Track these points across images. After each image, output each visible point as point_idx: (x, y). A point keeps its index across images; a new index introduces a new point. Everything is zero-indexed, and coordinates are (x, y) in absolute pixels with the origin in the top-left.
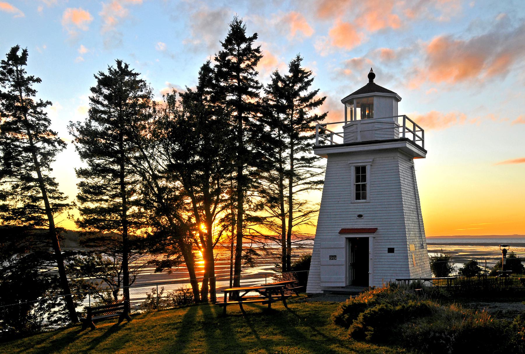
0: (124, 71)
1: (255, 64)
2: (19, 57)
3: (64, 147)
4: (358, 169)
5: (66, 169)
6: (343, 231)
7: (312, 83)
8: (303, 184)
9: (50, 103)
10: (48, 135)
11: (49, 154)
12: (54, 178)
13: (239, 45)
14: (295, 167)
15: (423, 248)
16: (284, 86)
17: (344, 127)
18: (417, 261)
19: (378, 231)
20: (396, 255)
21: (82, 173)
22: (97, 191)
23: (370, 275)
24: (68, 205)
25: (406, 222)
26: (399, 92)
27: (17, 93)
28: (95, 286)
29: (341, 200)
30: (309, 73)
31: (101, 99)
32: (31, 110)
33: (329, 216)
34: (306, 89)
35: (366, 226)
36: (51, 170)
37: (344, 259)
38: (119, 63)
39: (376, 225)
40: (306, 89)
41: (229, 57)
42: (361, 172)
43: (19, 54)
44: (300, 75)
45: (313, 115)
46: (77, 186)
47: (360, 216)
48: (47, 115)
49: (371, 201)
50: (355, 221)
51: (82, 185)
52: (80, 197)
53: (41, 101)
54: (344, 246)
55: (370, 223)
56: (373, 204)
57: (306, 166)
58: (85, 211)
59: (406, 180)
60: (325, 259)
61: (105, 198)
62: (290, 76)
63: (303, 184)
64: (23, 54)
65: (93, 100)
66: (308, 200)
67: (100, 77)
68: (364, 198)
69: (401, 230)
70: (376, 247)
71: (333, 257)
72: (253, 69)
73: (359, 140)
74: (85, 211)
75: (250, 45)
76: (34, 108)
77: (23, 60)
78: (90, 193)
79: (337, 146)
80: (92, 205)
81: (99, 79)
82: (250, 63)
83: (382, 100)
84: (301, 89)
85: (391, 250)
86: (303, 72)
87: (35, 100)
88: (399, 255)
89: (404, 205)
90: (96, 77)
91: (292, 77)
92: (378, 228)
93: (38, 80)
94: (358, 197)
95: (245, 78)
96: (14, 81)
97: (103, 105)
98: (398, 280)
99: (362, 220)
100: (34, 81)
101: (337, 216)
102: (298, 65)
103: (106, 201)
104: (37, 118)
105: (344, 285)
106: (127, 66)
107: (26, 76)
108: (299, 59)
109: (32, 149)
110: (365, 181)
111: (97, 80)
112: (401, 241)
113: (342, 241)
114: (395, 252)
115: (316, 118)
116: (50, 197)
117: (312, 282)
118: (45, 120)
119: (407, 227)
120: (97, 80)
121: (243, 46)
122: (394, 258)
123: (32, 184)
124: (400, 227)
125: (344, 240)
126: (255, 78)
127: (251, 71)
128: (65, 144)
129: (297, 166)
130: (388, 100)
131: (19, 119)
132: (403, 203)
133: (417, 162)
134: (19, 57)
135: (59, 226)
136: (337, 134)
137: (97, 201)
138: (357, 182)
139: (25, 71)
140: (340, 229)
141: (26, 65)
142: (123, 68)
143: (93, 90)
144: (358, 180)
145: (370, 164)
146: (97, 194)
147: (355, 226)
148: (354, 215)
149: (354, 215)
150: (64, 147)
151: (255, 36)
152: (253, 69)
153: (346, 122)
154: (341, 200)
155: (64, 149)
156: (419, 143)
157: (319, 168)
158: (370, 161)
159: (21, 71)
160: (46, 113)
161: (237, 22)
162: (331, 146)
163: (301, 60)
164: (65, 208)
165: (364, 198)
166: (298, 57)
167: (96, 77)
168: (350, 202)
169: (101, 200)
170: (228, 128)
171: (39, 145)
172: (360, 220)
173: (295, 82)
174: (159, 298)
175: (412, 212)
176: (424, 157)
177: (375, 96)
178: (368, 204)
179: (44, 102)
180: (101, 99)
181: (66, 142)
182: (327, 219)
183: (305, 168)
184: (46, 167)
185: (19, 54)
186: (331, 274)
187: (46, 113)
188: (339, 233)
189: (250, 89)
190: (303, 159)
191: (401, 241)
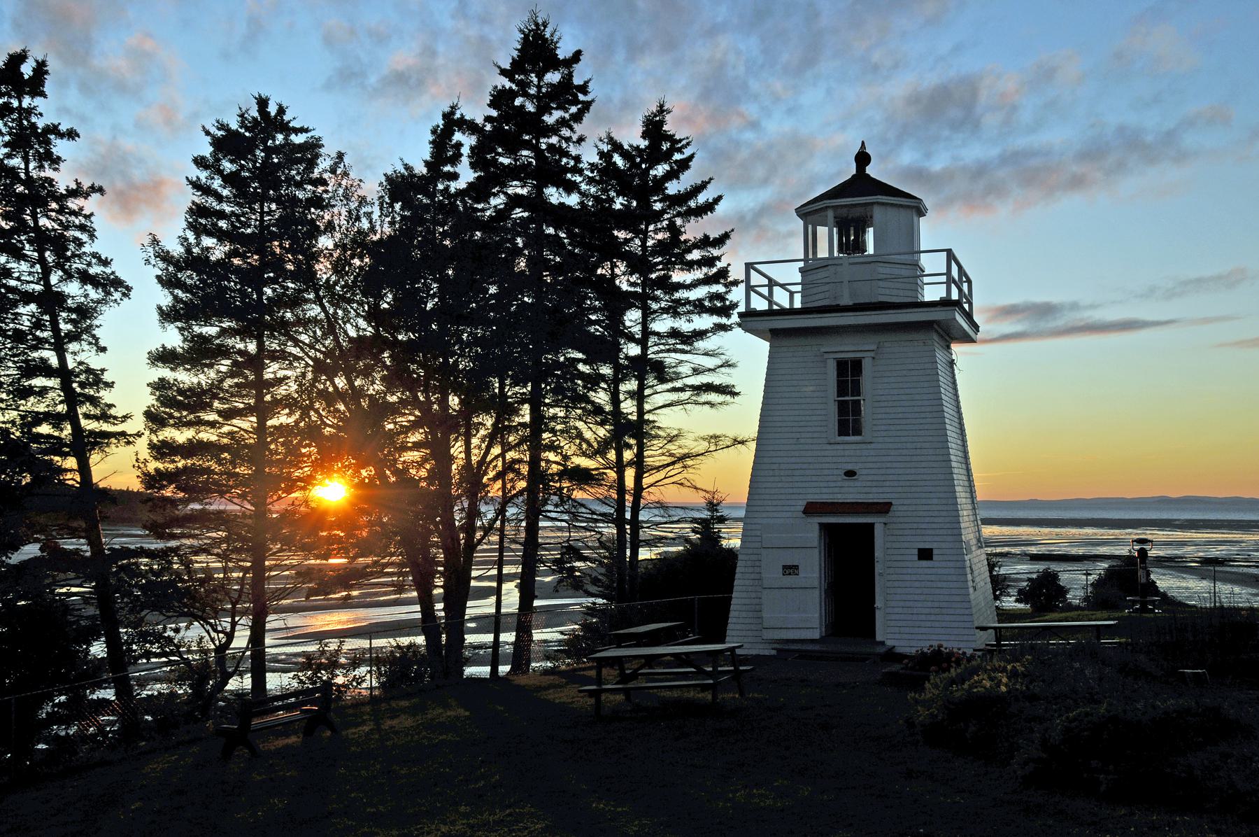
0: (268, 122)
1: (578, 117)
2: (26, 77)
3: (124, 295)
4: (842, 366)
5: (130, 346)
6: (812, 509)
8: (668, 391)
9: (101, 190)
10: (89, 264)
11: (84, 312)
12: (103, 370)
13: (540, 77)
16: (629, 169)
17: (801, 270)
20: (937, 564)
21: (165, 357)
22: (196, 400)
23: (877, 612)
24: (123, 434)
27: (16, 162)
28: (172, 634)
29: (804, 435)
30: (684, 142)
31: (217, 183)
32: (54, 205)
33: (777, 473)
34: (678, 178)
35: (862, 496)
36: (104, 349)
37: (816, 575)
38: (262, 103)
39: (888, 496)
40: (678, 178)
41: (518, 102)
42: (849, 372)
43: (27, 70)
44: (665, 146)
45: (700, 236)
46: (149, 390)
47: (850, 474)
48: (93, 219)
50: (839, 484)
51: (160, 386)
52: (149, 415)
53: (78, 184)
54: (816, 543)
55: (874, 490)
56: (880, 446)
57: (676, 351)
58: (162, 450)
60: (773, 574)
61: (212, 417)
62: (642, 147)
63: (668, 391)
64: (34, 70)
65: (196, 185)
66: (685, 428)
67: (220, 133)
68: (857, 432)
69: (946, 508)
70: (888, 545)
71: (790, 570)
72: (572, 129)
73: (846, 301)
74: (162, 450)
75: (570, 75)
76: (60, 199)
77: (36, 86)
78: (180, 406)
79: (783, 312)
80: (182, 436)
81: (213, 136)
82: (567, 116)
83: (891, 212)
84: (672, 175)
85: (925, 554)
86: (670, 138)
87: (63, 180)
88: (944, 564)
90: (208, 133)
91: (647, 147)
93: (72, 134)
94: (843, 430)
95: (551, 147)
96: (10, 134)
97: (220, 198)
100: (61, 135)
101: (797, 473)
102: (662, 123)
103: (212, 424)
104: (61, 224)
106: (281, 111)
107: (41, 123)
108: (662, 110)
109: (51, 301)
111: (209, 139)
112: (949, 532)
113: (811, 531)
114: (935, 557)
115: (705, 242)
116: (87, 416)
117: (738, 627)
118: (82, 228)
120: (209, 139)
121: (553, 77)
122: (934, 571)
123: (39, 382)
124: (944, 502)
125: (817, 527)
126: (573, 150)
127: (565, 132)
128: (129, 289)
129: (656, 348)
130: (903, 214)
131: (22, 227)
133: (957, 349)
134: (26, 77)
135: (101, 485)
136: (783, 286)
137: (189, 424)
139: (39, 110)
140: (805, 503)
141: (45, 96)
142: (273, 114)
143: (200, 162)
144: (842, 390)
145: (872, 354)
146: (192, 409)
147: (839, 496)
148: (836, 472)
149: (836, 472)
150: (124, 295)
152: (572, 129)
153: (806, 260)
154: (804, 435)
155: (126, 300)
157: (706, 354)
158: (873, 347)
159: (30, 111)
160: (92, 214)
162: (770, 313)
163: (669, 112)
164: (113, 440)
165: (857, 432)
166: (661, 106)
167: (208, 133)
168: (825, 441)
169: (199, 423)
170: (520, 262)
171: (73, 289)
172: (851, 484)
173: (653, 163)
174: (222, 649)
177: (878, 203)
178: (869, 446)
179: (86, 185)
180: (217, 183)
181: (129, 283)
182: (771, 479)
183: (673, 355)
184: (90, 343)
185: (27, 70)
186: (779, 609)
187: (92, 214)
188: (805, 512)
190: (674, 333)
191: (949, 532)
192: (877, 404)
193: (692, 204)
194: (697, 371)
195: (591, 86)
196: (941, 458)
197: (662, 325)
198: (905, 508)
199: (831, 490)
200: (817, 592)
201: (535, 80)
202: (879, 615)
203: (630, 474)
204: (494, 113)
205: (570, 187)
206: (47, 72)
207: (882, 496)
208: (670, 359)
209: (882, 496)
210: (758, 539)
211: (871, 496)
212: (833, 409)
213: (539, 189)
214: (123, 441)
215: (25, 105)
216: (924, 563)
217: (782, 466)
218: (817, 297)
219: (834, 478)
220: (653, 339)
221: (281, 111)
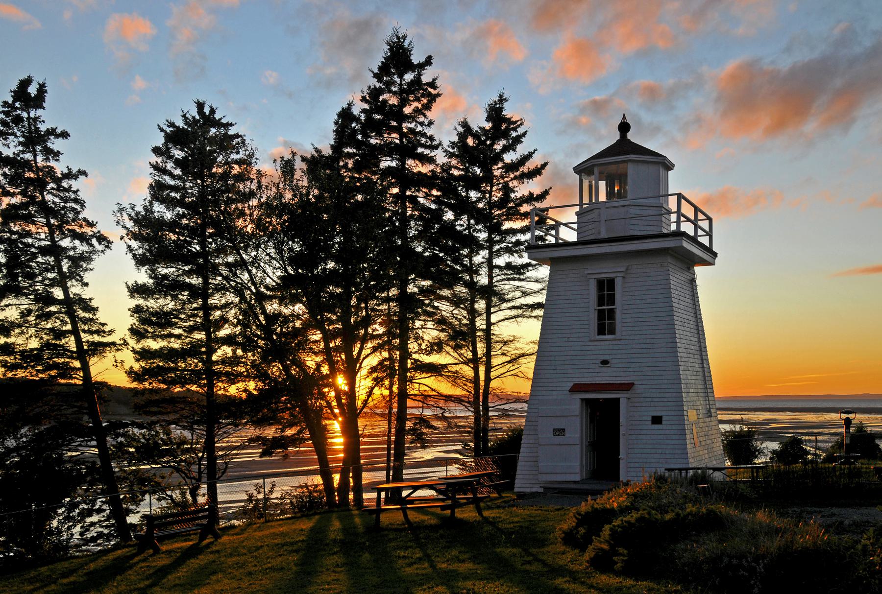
1: (428, 107)
2: (33, 95)
3: (107, 247)
4: (601, 284)
5: (112, 285)
6: (577, 388)
7: (523, 139)
8: (509, 308)
9: (84, 173)
12: (90, 299)
13: (401, 76)
14: (495, 279)
15: (711, 416)
16: (478, 145)
17: (577, 214)
18: (701, 439)
19: (634, 387)
21: (137, 290)
25: (681, 372)
26: (670, 155)
27: (28, 156)
28: (160, 480)
31: (170, 166)
32: (52, 185)
34: (514, 150)
35: (614, 379)
36: (86, 284)
37: (578, 435)
38: (200, 106)
40: (514, 150)
42: (606, 288)
43: (33, 90)
45: (526, 193)
46: (130, 313)
47: (605, 362)
48: (79, 193)
49: (624, 337)
50: (597, 370)
51: (137, 310)
52: (133, 331)
53: (69, 170)
54: (577, 412)
55: (622, 374)
56: (626, 342)
57: (514, 279)
58: (144, 354)
59: (682, 303)
60: (546, 435)
61: (177, 331)
62: (487, 128)
63: (509, 308)
64: (38, 90)
65: (156, 167)
66: (518, 334)
67: (169, 130)
68: (612, 332)
71: (559, 432)
72: (425, 116)
73: (604, 235)
74: (144, 354)
75: (420, 75)
76: (57, 181)
77: (38, 101)
78: (151, 323)
79: (567, 244)
80: (154, 345)
81: (166, 132)
82: (420, 106)
83: (643, 168)
84: (506, 149)
85: (657, 420)
86: (508, 121)
87: (60, 168)
89: (679, 345)
90: (162, 130)
91: (491, 128)
92: (636, 383)
93: (65, 135)
94: (601, 331)
95: (412, 131)
96: (23, 136)
97: (173, 177)
98: (669, 470)
99: (609, 370)
100: (57, 136)
102: (501, 109)
104: (61, 198)
105: (577, 478)
106: (213, 111)
108: (502, 99)
109: (54, 250)
110: (613, 303)
111: (163, 134)
113: (575, 405)
114: (664, 422)
115: (530, 198)
116: (84, 331)
117: (524, 472)
118: (76, 201)
119: (683, 382)
120: (163, 134)
121: (409, 77)
125: (578, 402)
126: (429, 132)
127: (421, 119)
128: (109, 242)
129: (499, 278)
130: (652, 168)
132: (678, 340)
134: (33, 95)
135: (99, 380)
136: (566, 225)
137: (163, 337)
138: (599, 306)
139: (42, 118)
141: (44, 108)
142: (207, 114)
143: (156, 151)
145: (622, 274)
146: (163, 326)
147: (597, 379)
148: (594, 361)
151: (429, 61)
152: (425, 116)
153: (581, 204)
156: (705, 240)
157: (537, 281)
158: (623, 269)
160: (78, 190)
161: (398, 38)
162: (556, 245)
163: (506, 100)
165: (612, 332)
166: (501, 96)
167: (162, 130)
168: (587, 339)
170: (381, 216)
172: (604, 370)
173: (495, 138)
174: (266, 499)
175: (692, 356)
176: (713, 264)
178: (619, 342)
179: (74, 171)
180: (170, 166)
183: (512, 282)
184: (77, 280)
185: (33, 90)
187: (78, 190)
188: (570, 391)
189: (420, 150)
190: (509, 266)
192: (625, 312)
193: (525, 170)
194: (525, 294)
195: (438, 83)
196: (671, 350)
197: (501, 261)
198: (644, 387)
199: (590, 375)
200: (578, 448)
201: (398, 80)
202: (622, 465)
203: (482, 369)
204: (367, 106)
205: (425, 159)
206: (46, 92)
207: (628, 378)
208: (506, 287)
209: (628, 378)
210: (536, 411)
211: (604, 379)
212: (594, 316)
213: (402, 161)
214: (114, 349)
215: (32, 115)
216: (656, 426)
217: (557, 358)
218: (587, 233)
219: (593, 366)
220: (496, 271)
221: (213, 111)
